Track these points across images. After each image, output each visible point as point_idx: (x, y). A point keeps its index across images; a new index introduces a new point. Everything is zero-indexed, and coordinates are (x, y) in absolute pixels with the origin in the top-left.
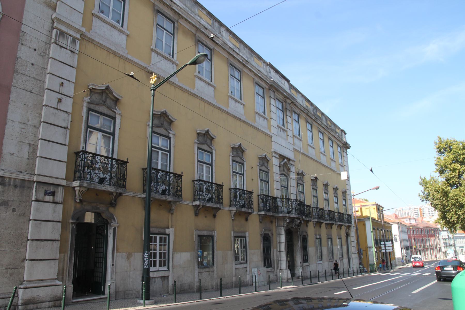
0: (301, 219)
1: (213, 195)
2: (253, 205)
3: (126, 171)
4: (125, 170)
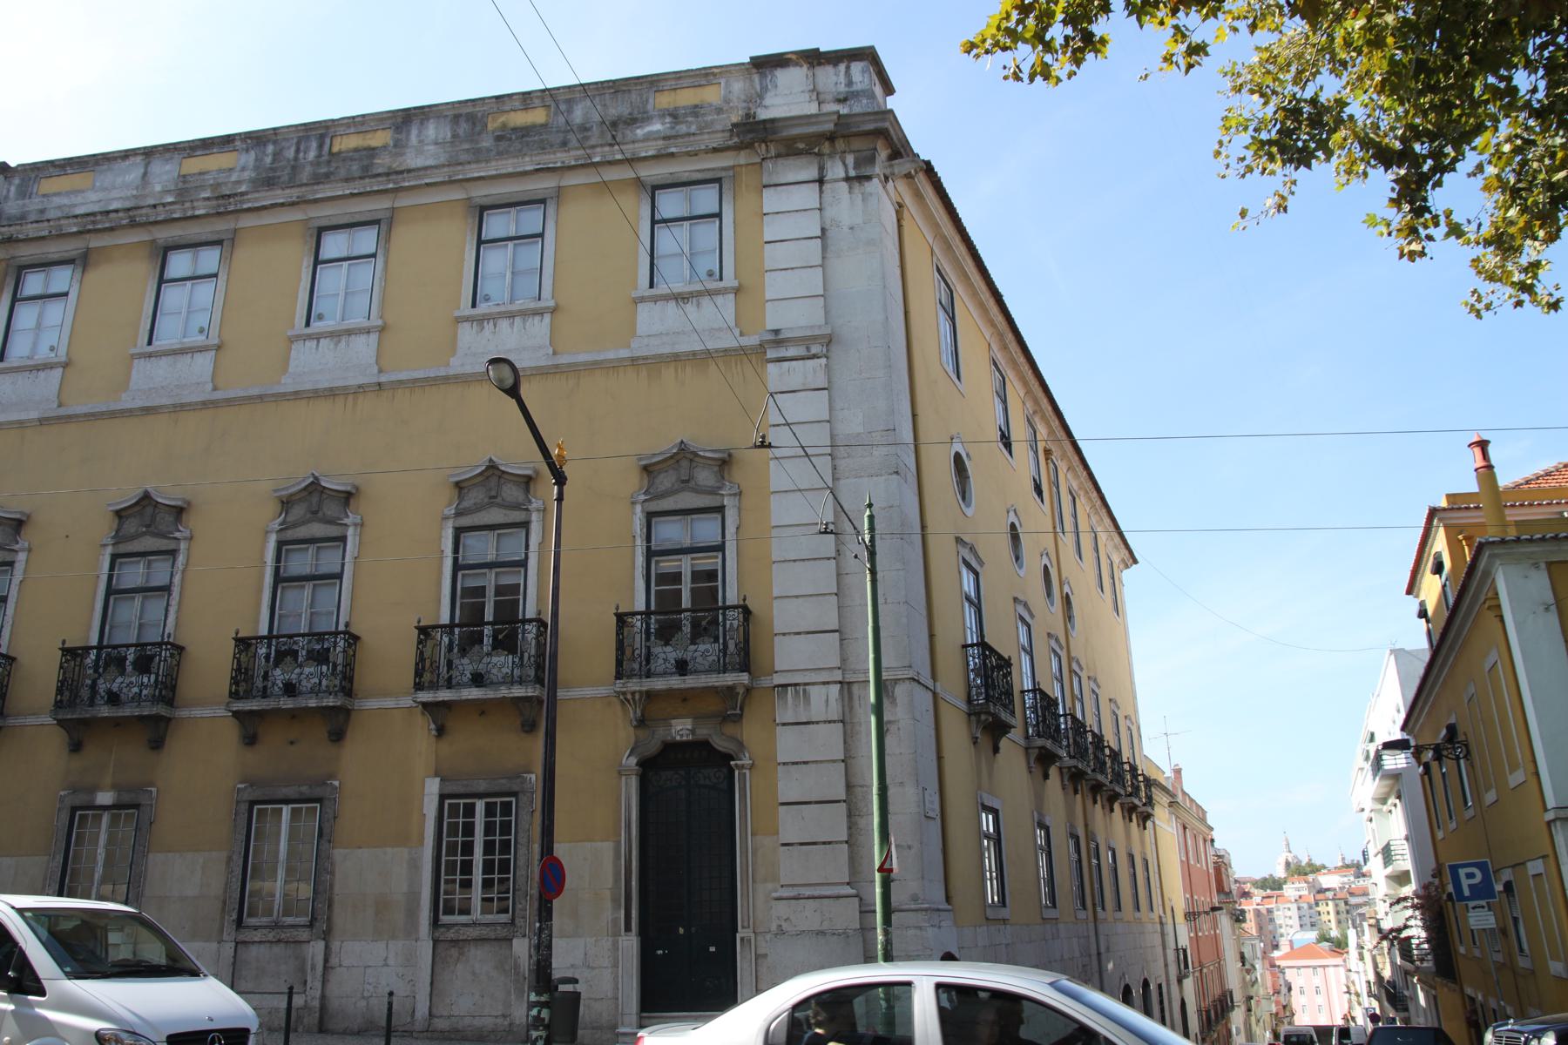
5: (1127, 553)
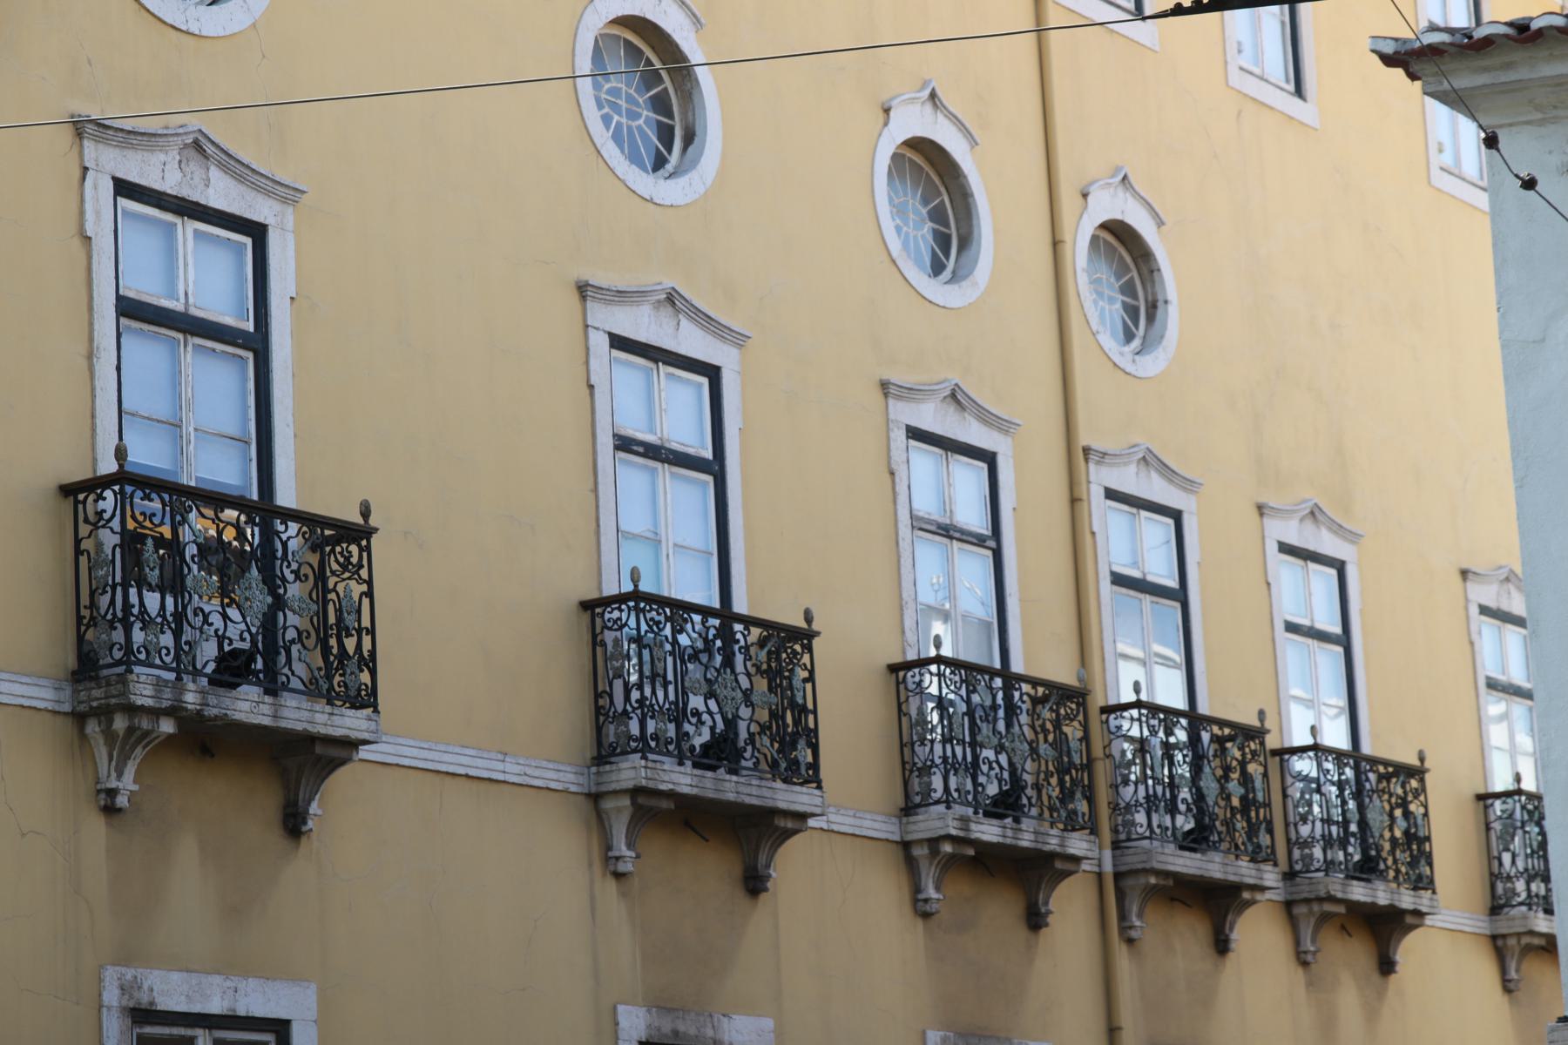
0: (692, 758)
1: (745, 712)
2: (1430, 865)
3: (366, 601)
4: (805, 680)
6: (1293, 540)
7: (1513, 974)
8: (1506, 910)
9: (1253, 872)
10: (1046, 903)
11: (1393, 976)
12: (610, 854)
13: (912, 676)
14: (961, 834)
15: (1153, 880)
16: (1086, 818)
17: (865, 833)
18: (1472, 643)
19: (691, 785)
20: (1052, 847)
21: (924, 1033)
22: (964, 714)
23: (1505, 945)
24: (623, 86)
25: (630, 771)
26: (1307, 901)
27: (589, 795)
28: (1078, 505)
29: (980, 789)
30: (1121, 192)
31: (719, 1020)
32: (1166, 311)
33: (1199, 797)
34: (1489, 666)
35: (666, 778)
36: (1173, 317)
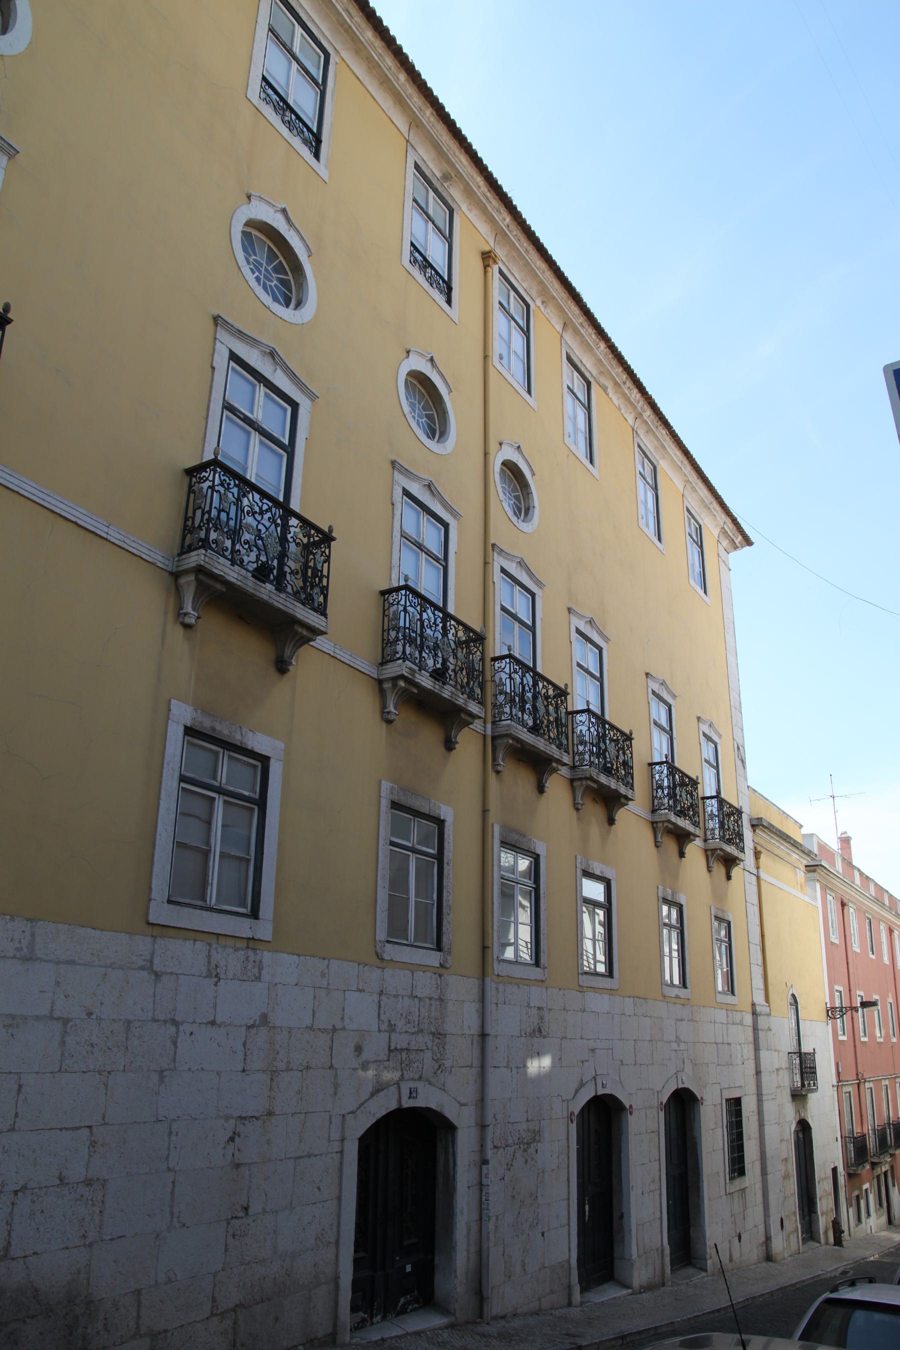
5: (729, 521)
6: (582, 629)
7: (659, 839)
8: (658, 811)
9: (558, 753)
10: (456, 737)
11: (614, 826)
12: (181, 612)
13: (392, 597)
14: (410, 677)
15: (511, 741)
16: (480, 697)
17: (356, 666)
18: (649, 703)
19: (237, 579)
20: (460, 703)
21: (380, 781)
22: (417, 619)
23: (657, 826)
24: (264, 263)
25: (196, 558)
26: (580, 779)
27: (171, 573)
28: (487, 565)
29: (423, 659)
30: (516, 452)
31: (246, 732)
32: (534, 511)
33: (535, 708)
34: (654, 716)
35: (219, 567)
36: (537, 513)
